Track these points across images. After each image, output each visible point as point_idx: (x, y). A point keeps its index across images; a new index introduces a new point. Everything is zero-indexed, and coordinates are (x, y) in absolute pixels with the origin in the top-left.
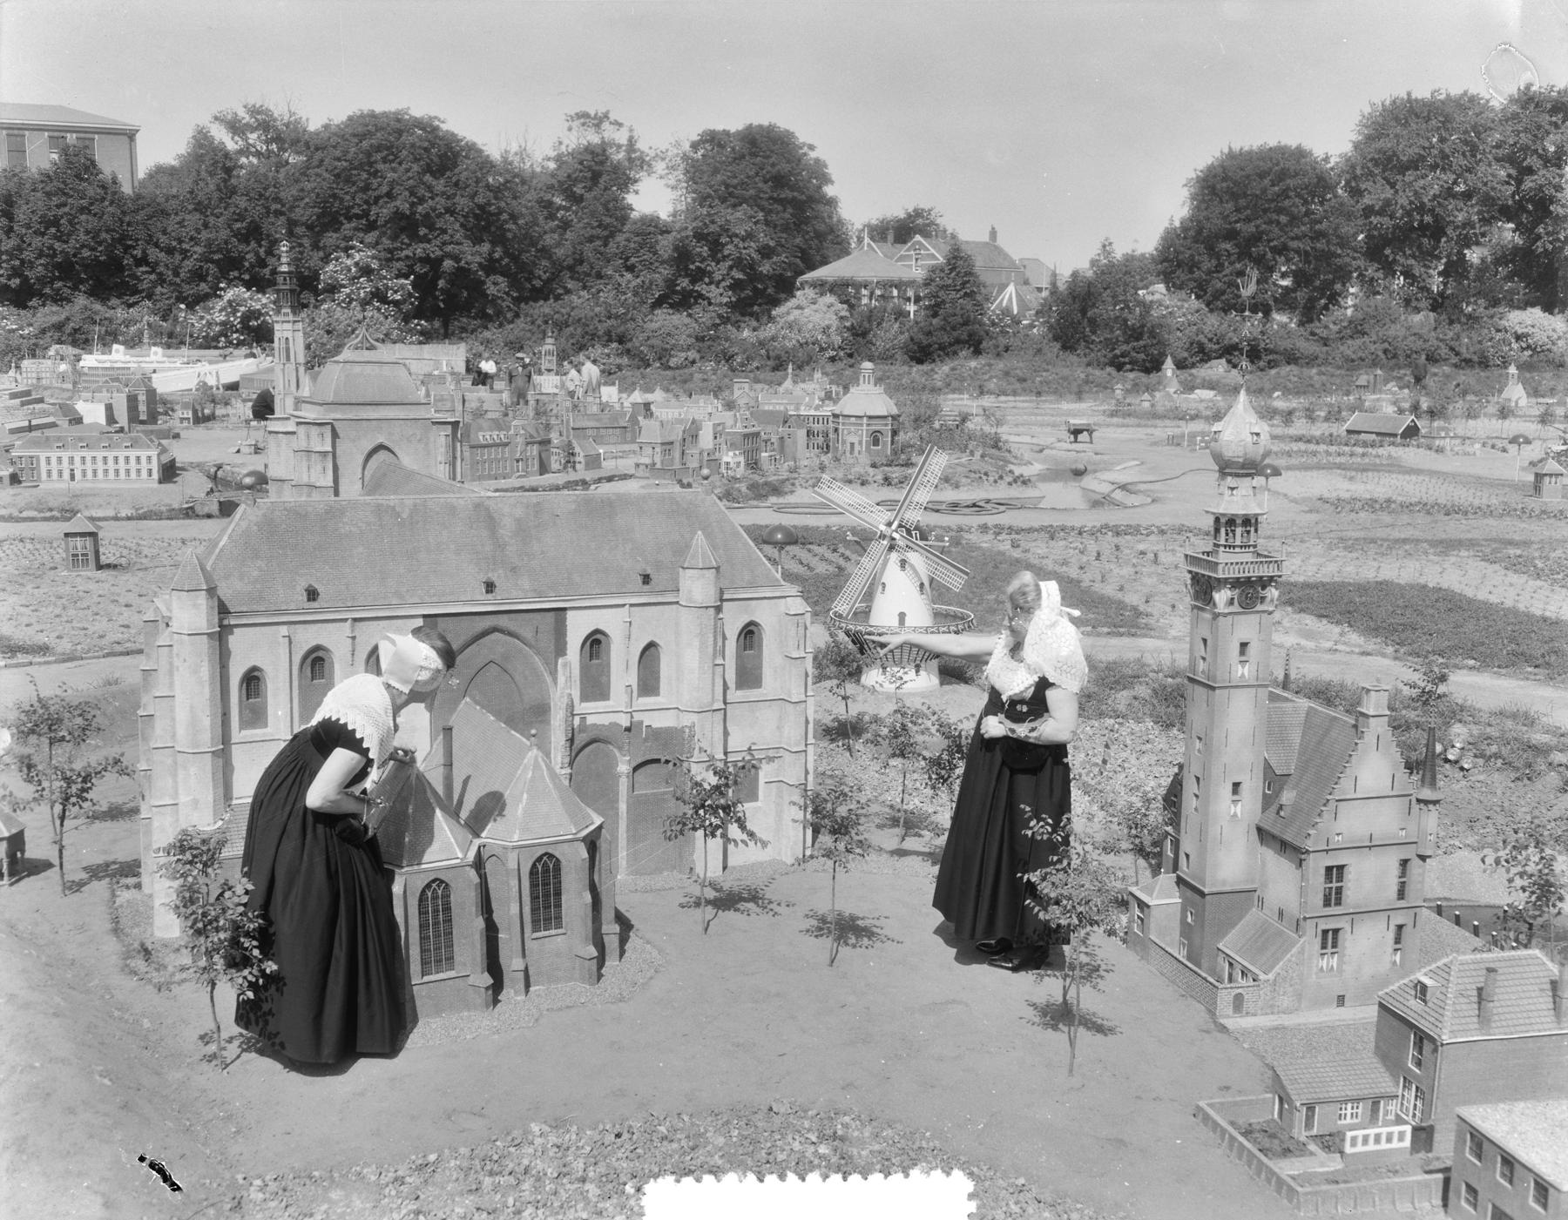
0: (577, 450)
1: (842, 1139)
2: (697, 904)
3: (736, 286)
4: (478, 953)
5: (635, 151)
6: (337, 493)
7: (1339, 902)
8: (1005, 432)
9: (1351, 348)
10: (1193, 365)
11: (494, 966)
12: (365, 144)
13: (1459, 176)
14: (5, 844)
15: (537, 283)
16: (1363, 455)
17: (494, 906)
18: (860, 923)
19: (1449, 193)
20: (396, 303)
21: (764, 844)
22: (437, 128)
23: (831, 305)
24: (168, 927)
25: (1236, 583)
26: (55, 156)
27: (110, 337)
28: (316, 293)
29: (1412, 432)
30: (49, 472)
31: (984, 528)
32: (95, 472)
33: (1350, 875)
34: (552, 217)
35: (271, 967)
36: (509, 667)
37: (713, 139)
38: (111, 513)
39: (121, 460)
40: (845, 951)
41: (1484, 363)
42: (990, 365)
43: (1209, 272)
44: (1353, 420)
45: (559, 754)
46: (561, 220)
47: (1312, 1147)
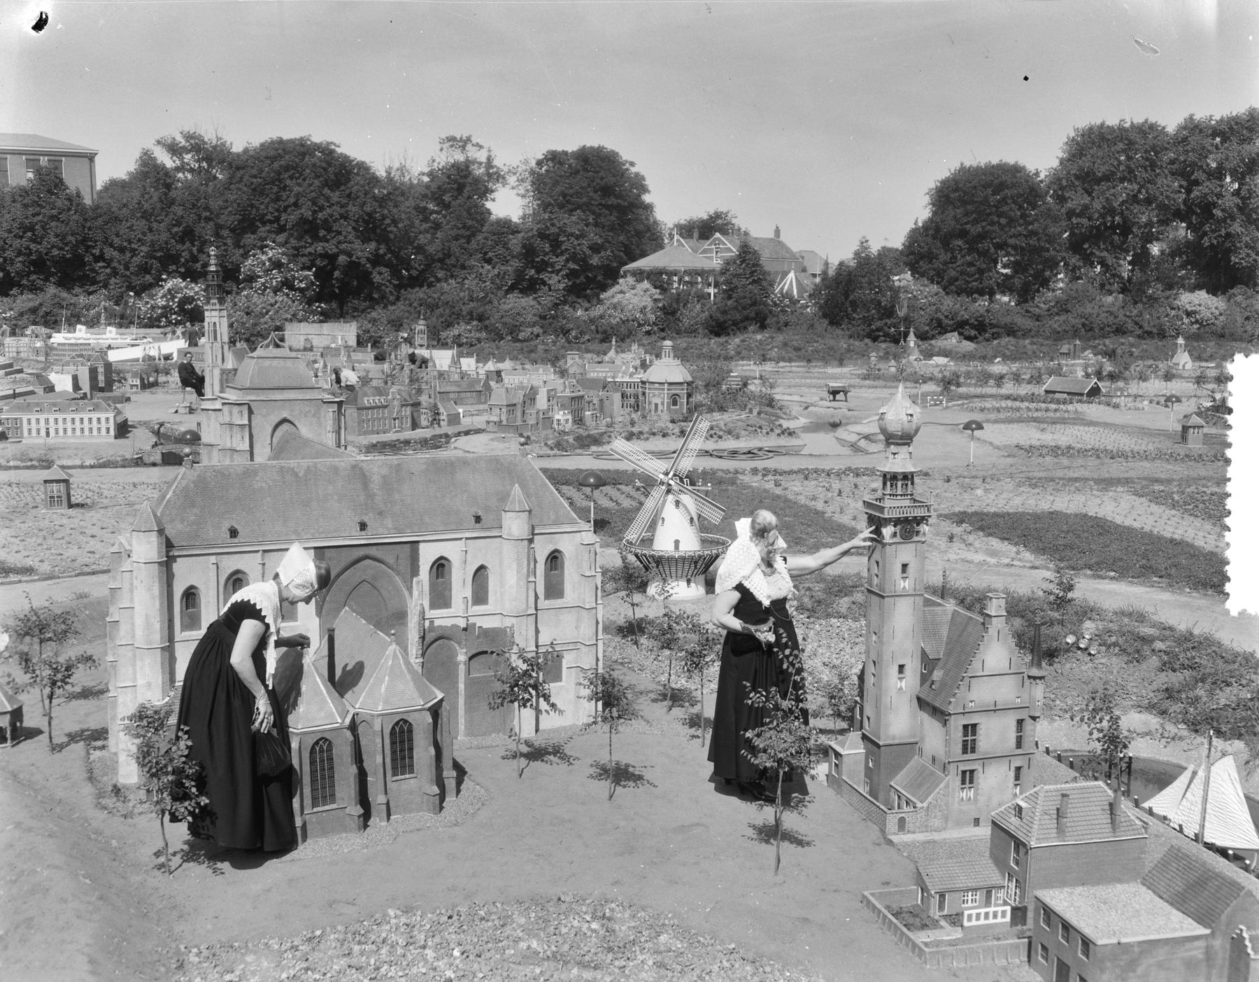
0: (442, 410)
1: (609, 919)
2: (514, 757)
3: (572, 274)
4: (353, 792)
5: (492, 167)
6: (252, 459)
7: (973, 750)
8: (779, 395)
9: (1056, 323)
10: (933, 337)
11: (364, 801)
12: (276, 165)
13: (1142, 187)
14: (8, 717)
15: (414, 273)
16: (1056, 410)
17: (364, 757)
18: (631, 769)
19: (1134, 199)
20: (301, 290)
21: (561, 712)
22: (332, 152)
23: (647, 290)
24: (129, 773)
25: (897, 522)
26: (31, 175)
27: (74, 320)
28: (238, 282)
29: (1095, 392)
30: (30, 430)
31: (755, 471)
32: (65, 430)
33: (981, 731)
34: (426, 220)
35: (204, 801)
36: (378, 585)
37: (554, 158)
38: (78, 462)
39: (86, 421)
40: (619, 789)
41: (1162, 335)
42: (772, 338)
43: (945, 263)
44: (1050, 382)
45: (414, 648)
46: (434, 222)
47: (943, 923)
